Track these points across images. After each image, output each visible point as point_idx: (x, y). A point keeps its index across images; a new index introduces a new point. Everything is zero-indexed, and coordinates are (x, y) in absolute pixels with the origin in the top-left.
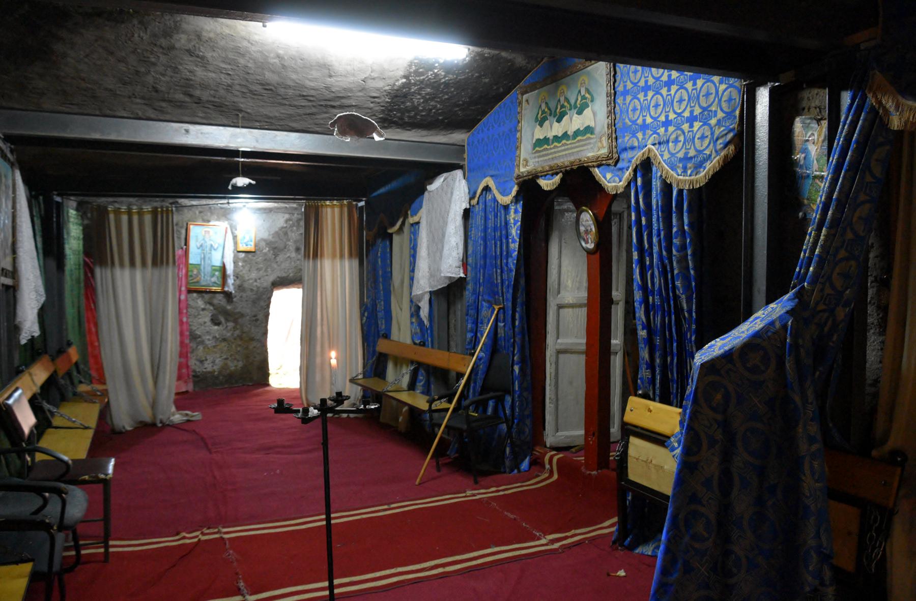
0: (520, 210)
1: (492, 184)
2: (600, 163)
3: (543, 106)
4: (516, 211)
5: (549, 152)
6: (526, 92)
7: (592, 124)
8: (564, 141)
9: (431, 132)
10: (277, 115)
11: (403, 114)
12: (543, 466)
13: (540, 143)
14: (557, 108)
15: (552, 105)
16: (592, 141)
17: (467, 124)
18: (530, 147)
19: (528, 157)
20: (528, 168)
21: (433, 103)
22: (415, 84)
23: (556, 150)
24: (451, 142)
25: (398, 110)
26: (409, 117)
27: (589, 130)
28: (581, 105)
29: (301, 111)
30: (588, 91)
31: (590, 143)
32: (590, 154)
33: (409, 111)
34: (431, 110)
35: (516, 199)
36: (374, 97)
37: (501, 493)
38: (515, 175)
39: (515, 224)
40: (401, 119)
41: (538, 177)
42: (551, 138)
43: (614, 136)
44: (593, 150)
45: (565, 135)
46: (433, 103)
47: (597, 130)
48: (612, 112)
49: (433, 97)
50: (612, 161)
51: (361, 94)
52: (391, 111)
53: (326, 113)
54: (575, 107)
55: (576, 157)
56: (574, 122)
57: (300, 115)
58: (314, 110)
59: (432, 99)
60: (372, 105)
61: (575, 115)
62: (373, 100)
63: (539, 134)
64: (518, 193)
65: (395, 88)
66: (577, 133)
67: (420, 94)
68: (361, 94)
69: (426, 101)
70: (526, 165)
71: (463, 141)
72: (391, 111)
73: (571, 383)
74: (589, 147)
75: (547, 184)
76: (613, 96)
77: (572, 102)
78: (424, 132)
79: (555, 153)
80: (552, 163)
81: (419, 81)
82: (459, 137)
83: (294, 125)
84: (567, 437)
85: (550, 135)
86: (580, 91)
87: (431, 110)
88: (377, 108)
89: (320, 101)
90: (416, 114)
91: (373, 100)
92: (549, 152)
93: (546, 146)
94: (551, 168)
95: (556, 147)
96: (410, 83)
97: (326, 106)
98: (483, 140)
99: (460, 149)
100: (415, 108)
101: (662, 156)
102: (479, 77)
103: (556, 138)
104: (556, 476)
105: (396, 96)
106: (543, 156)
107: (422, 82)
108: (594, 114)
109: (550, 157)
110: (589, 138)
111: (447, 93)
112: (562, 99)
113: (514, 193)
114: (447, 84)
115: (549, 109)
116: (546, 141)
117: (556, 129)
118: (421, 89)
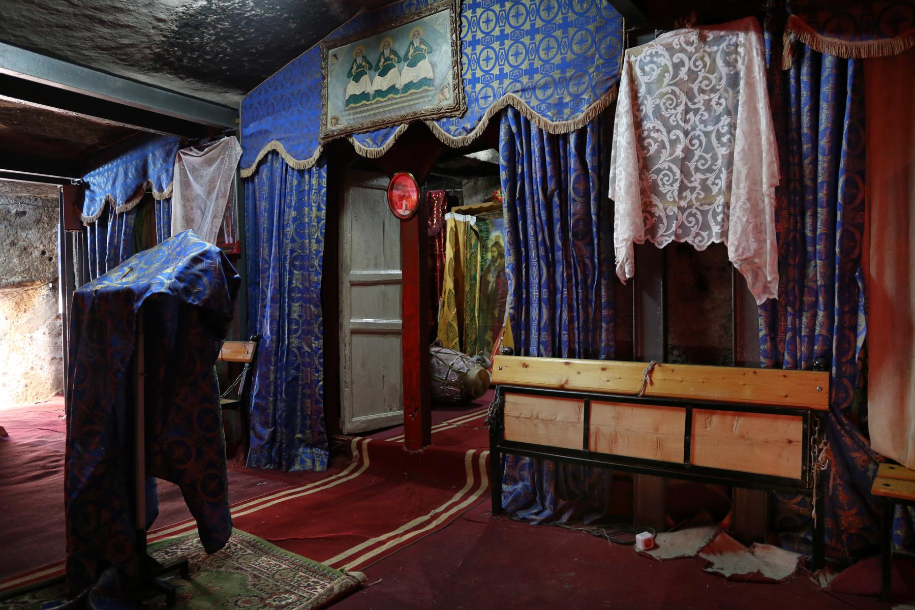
0: (325, 175)
1: (280, 147)
2: (440, 115)
3: (359, 60)
4: (320, 177)
5: (370, 107)
6: (333, 47)
7: (430, 75)
8: (390, 96)
9: (205, 86)
10: (15, 16)
11: (185, 53)
12: (349, 455)
13: (354, 98)
14: (379, 61)
15: (372, 58)
16: (430, 93)
17: (244, 81)
18: (341, 104)
19: (338, 115)
20: (339, 127)
21: (224, 45)
22: (215, 12)
23: (379, 105)
24: (224, 102)
25: (182, 46)
26: (191, 59)
27: (425, 82)
28: (414, 57)
29: (53, 19)
30: (422, 42)
31: (428, 96)
32: (429, 107)
33: (193, 50)
34: (218, 53)
35: (319, 163)
36: (160, 20)
37: (345, 480)
38: (322, 136)
39: (531, 114)
40: (180, 60)
41: (350, 136)
42: (372, 93)
43: (461, 87)
44: (426, 104)
45: (393, 89)
46: (224, 45)
47: (437, 82)
48: (458, 63)
49: (226, 36)
50: (459, 110)
51: (144, 10)
52: (172, 45)
53: (88, 30)
54: (406, 58)
55: (413, 109)
56: (402, 75)
57: (49, 26)
58: (74, 22)
59: (225, 39)
60: (152, 31)
61: (406, 67)
62: (156, 23)
63: (354, 89)
64: (322, 155)
65: (191, 12)
66: (408, 86)
67: (215, 28)
68: (144, 10)
69: (219, 38)
70: (337, 123)
71: (238, 103)
72: (172, 45)
73: (363, 365)
74: (426, 99)
75: (363, 146)
76: (458, 49)
77: (402, 53)
78: (198, 85)
79: (378, 108)
80: (375, 119)
81: (221, 8)
82: (233, 98)
83: (35, 39)
84: (362, 422)
85: (371, 90)
86: (412, 43)
87: (218, 53)
88: (157, 38)
89: (86, 8)
90: (199, 57)
91: (156, 23)
92: (370, 107)
93: (364, 102)
94: (375, 124)
95: (378, 102)
96: (210, 8)
97: (92, 18)
98: (266, 101)
99: (233, 112)
100: (201, 46)
101: (528, 103)
102: (287, 19)
103: (379, 93)
104: (367, 462)
105: (187, 25)
106: (361, 112)
107: (224, 10)
108: (433, 65)
109: (371, 112)
110: (427, 91)
111: (243, 34)
112: (387, 53)
113: (316, 154)
114: (249, 20)
115: (368, 62)
116: (365, 96)
117: (381, 83)
118: (218, 21)
